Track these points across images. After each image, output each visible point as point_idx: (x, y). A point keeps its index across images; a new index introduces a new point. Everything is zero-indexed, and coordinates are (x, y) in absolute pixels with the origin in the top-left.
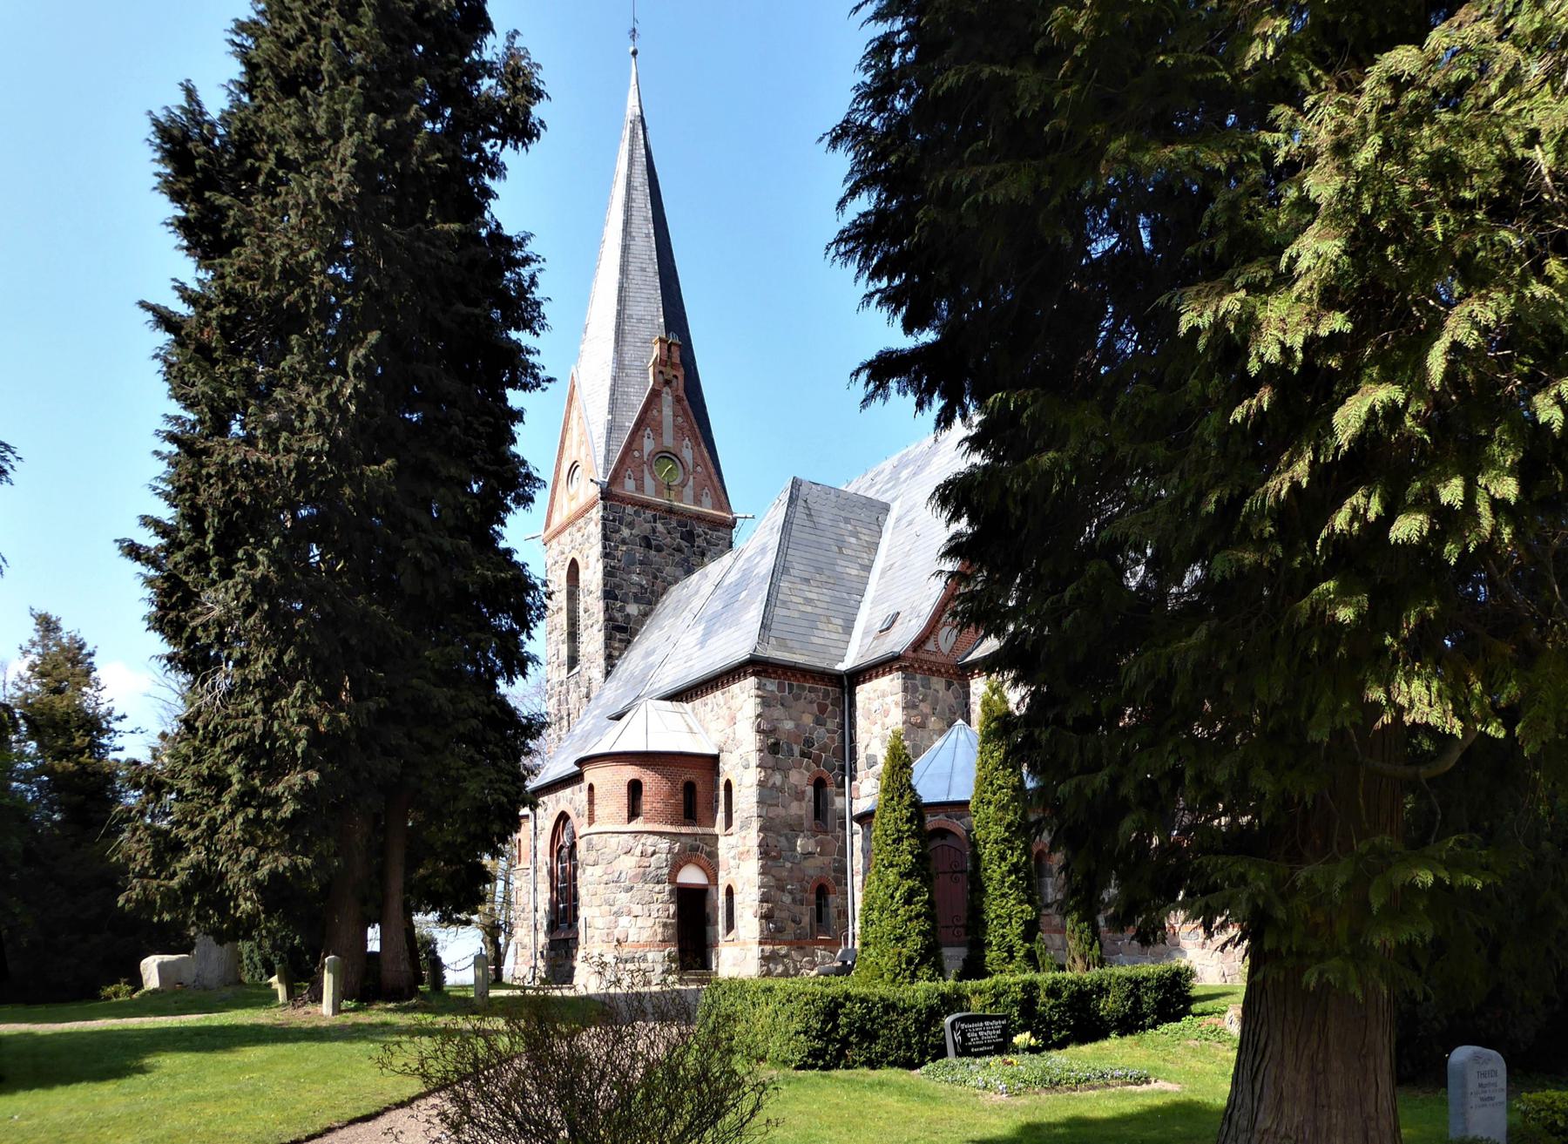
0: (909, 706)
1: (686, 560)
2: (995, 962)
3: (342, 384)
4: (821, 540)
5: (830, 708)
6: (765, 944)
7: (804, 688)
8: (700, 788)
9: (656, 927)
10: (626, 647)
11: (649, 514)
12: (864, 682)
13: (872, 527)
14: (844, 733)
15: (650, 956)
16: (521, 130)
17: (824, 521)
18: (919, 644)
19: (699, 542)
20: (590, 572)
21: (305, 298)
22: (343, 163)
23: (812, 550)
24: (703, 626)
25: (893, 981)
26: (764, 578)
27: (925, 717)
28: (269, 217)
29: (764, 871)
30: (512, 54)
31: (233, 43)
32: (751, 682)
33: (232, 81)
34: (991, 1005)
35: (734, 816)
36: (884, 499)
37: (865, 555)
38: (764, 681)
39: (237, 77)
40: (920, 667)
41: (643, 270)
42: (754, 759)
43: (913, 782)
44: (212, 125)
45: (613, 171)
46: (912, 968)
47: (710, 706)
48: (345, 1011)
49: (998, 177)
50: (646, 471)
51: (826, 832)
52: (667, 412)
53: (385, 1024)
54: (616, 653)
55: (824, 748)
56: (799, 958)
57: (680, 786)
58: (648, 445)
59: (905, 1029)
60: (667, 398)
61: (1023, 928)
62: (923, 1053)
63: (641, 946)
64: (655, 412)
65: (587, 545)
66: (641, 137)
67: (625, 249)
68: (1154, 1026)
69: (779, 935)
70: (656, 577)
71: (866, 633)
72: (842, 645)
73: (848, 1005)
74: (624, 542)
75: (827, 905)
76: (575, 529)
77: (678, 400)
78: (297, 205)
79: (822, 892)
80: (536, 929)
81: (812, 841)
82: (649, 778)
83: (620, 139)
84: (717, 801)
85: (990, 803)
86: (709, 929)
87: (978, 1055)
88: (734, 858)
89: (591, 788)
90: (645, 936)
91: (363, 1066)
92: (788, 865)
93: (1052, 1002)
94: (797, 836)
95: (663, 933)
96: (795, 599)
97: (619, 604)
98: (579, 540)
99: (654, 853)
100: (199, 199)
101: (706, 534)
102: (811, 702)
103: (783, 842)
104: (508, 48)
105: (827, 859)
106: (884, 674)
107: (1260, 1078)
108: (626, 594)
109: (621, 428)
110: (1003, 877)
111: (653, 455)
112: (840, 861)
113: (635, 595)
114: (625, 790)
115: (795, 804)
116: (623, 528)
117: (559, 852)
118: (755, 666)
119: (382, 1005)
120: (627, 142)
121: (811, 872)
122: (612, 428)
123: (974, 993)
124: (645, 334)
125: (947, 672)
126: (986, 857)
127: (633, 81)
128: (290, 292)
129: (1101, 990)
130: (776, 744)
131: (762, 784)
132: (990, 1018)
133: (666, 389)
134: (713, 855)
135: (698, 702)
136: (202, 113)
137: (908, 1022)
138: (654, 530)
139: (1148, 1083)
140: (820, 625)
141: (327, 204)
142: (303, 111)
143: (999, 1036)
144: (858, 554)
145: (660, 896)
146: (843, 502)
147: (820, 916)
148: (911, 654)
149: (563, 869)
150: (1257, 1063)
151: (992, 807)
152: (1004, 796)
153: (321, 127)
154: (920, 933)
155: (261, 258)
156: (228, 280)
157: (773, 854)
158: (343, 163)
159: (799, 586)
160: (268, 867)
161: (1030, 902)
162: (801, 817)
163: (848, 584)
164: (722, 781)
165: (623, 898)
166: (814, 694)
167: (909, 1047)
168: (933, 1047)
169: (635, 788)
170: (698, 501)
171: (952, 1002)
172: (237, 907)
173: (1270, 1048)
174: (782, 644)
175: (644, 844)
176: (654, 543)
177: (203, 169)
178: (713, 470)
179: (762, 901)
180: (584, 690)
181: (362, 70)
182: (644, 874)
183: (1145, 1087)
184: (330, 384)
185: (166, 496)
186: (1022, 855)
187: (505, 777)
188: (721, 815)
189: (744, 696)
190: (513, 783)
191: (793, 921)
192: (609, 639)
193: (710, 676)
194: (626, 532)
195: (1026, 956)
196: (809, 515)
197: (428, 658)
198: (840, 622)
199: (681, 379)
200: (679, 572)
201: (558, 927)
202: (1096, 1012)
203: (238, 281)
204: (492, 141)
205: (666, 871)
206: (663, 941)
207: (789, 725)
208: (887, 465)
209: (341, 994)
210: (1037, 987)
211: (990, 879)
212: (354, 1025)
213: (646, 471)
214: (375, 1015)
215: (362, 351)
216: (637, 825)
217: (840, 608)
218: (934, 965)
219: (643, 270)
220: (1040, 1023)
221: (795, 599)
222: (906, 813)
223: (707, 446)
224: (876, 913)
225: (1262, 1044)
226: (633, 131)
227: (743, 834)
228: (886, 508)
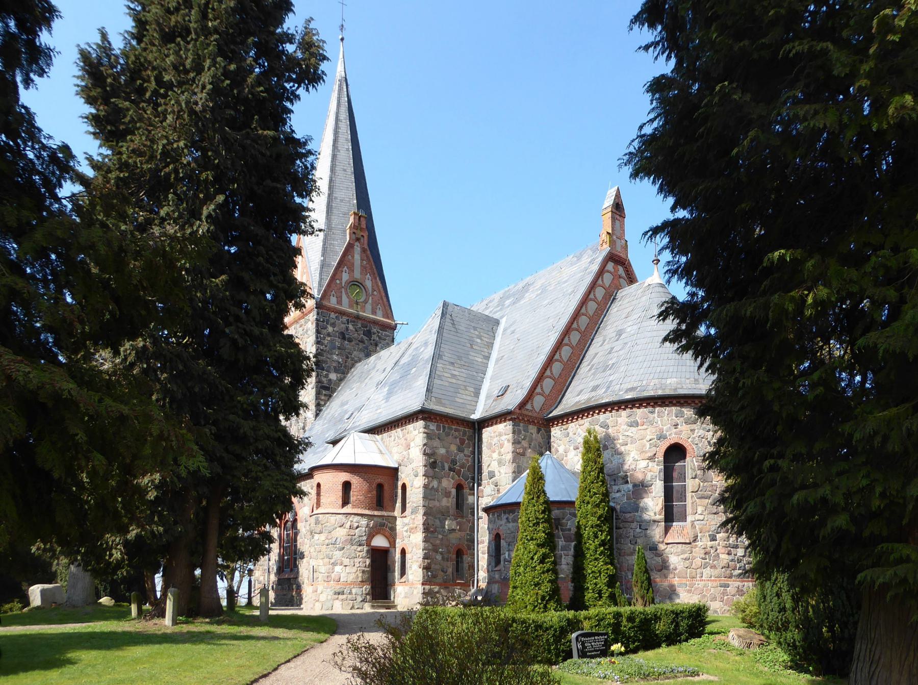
0: (516, 442)
1: (366, 348)
2: (591, 600)
3: (199, 226)
4: (460, 339)
5: (467, 442)
6: (426, 584)
7: (452, 429)
8: (386, 487)
9: (358, 573)
10: (328, 400)
11: (345, 319)
12: (487, 427)
13: (489, 333)
14: (474, 457)
15: (354, 591)
16: (312, 77)
17: (462, 328)
18: (522, 405)
19: (374, 337)
21: (176, 171)
22: (204, 87)
23: (454, 345)
24: (387, 389)
25: (533, 610)
26: (427, 361)
27: (525, 449)
28: (153, 118)
29: (426, 540)
30: (308, 32)
31: (129, 7)
32: (420, 424)
33: (126, 32)
34: (596, 626)
35: (407, 505)
36: (496, 316)
37: (486, 350)
38: (429, 423)
39: (130, 29)
40: (523, 419)
41: (345, 170)
42: (421, 471)
43: (545, 489)
44: (117, 57)
45: (327, 109)
46: (545, 602)
47: (393, 438)
48: (180, 623)
49: (816, 113)
50: (343, 292)
51: (462, 517)
52: (357, 257)
53: (208, 632)
54: (322, 403)
55: (462, 466)
56: (445, 594)
57: (374, 486)
58: (345, 277)
59: (548, 640)
60: (357, 249)
61: (607, 579)
62: (557, 656)
63: (348, 584)
64: (350, 257)
65: (306, 335)
66: (345, 90)
67: (334, 157)
68: (686, 640)
69: (434, 580)
70: (347, 358)
71: (488, 397)
72: (473, 403)
73: (515, 625)
74: (329, 335)
75: (462, 562)
76: (298, 325)
77: (364, 251)
78: (173, 112)
79: (459, 553)
80: (269, 572)
81: (454, 522)
82: (355, 481)
83: (332, 90)
84: (396, 496)
85: (588, 503)
86: (389, 574)
87: (593, 657)
88: (406, 531)
89: (319, 485)
90: (351, 578)
91: (210, 660)
92: (440, 536)
93: (630, 625)
94: (446, 519)
95: (362, 577)
96: (446, 375)
97: (325, 373)
98: (301, 332)
99: (357, 527)
100: (106, 102)
101: (378, 332)
102: (456, 438)
103: (438, 523)
104: (306, 28)
105: (463, 534)
106: (500, 423)
107: (875, 678)
108: (329, 367)
109: (329, 265)
110: (596, 548)
111: (348, 283)
112: (470, 535)
113: (335, 368)
114: (340, 487)
115: (445, 500)
116: (329, 326)
117: (285, 524)
118: (424, 414)
119: (201, 620)
120: (336, 92)
121: (454, 541)
122: (323, 265)
123: (585, 618)
124: (345, 209)
125: (538, 422)
126: (585, 536)
127: (341, 56)
128: (167, 165)
129: (656, 618)
130: (435, 462)
131: (426, 487)
132: (598, 635)
133: (357, 244)
134: (393, 529)
135: (385, 435)
136: (111, 49)
137: (549, 636)
138: (347, 329)
139: (698, 675)
140: (461, 391)
141: (192, 112)
142: (177, 53)
143: (603, 645)
144: (482, 349)
145: (361, 553)
146: (473, 317)
147: (458, 568)
148: (518, 411)
149: (288, 535)
150: (873, 669)
151: (590, 506)
152: (597, 499)
153: (188, 63)
154: (550, 581)
155: (149, 143)
156: (125, 156)
157: (432, 529)
158: (204, 87)
159: (448, 367)
160: (135, 532)
161: (612, 564)
162: (448, 507)
163: (477, 367)
164: (400, 484)
165: (338, 554)
166: (459, 431)
167: (549, 651)
168: (563, 651)
169: (347, 486)
170: (374, 313)
171: (573, 625)
172: (111, 555)
173: (882, 660)
174: (439, 401)
175: (351, 521)
176: (347, 336)
177: (111, 85)
178: (383, 294)
179: (424, 558)
180: (301, 425)
181: (216, 31)
182: (351, 540)
183: (696, 679)
184: (192, 226)
186: (607, 535)
187: (285, 477)
188: (399, 505)
189: (416, 432)
190: (291, 481)
191: (443, 571)
192: (318, 394)
193: (395, 419)
194: (330, 329)
195: (609, 596)
196: (453, 324)
197: (239, 402)
198: (472, 389)
199: (366, 237)
200: (362, 355)
201: (283, 571)
202: (654, 632)
203: (131, 157)
204: (291, 84)
205: (365, 538)
206: (362, 582)
207: (442, 451)
208: (497, 297)
209: (178, 612)
210: (622, 616)
211: (588, 549)
212: (188, 632)
213: (343, 292)
214: (200, 626)
215: (212, 207)
216: (348, 509)
217: (472, 381)
218: (557, 601)
219: (345, 170)
220: (623, 638)
221: (446, 375)
222: (542, 508)
223: (380, 279)
224: (522, 569)
225: (877, 657)
226: (340, 86)
227: (413, 517)
228: (497, 322)
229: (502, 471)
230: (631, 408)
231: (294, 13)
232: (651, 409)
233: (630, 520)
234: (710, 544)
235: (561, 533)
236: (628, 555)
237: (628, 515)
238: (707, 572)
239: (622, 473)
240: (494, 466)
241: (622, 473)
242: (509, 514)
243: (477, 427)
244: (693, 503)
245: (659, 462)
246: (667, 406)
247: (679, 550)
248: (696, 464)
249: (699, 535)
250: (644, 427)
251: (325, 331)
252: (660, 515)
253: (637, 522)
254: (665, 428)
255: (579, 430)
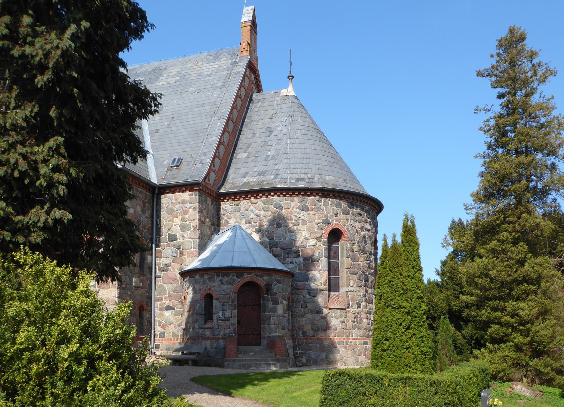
51: (144, 275)
94: (133, 276)
106: (184, 191)
229: (186, 235)
230: (303, 195)
232: (318, 198)
233: (301, 287)
234: (357, 310)
235: (270, 297)
236: (299, 317)
237: (299, 284)
238: (356, 332)
239: (294, 248)
240: (176, 230)
241: (294, 248)
242: (223, 277)
243: (156, 192)
244: (347, 277)
245: (324, 242)
246: (331, 197)
247: (338, 314)
248: (349, 246)
249: (351, 303)
250: (313, 212)
252: (325, 285)
253: (307, 289)
254: (328, 215)
255: (252, 207)
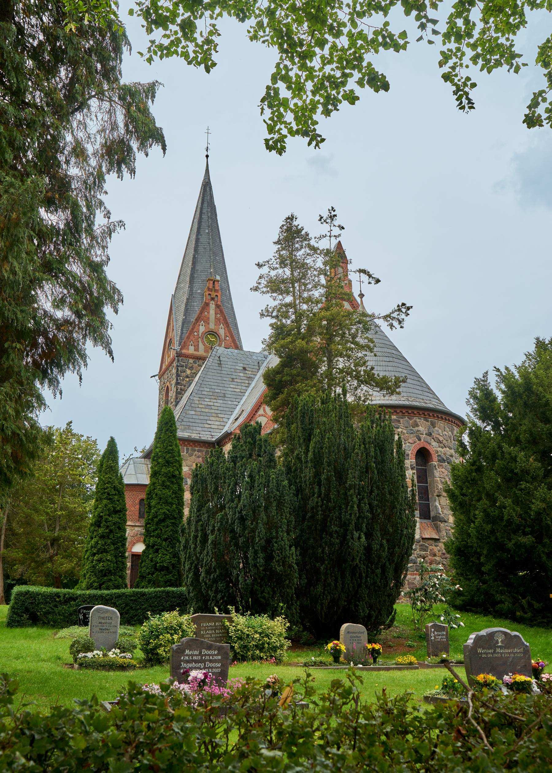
20: (172, 392)
57: (137, 501)
58: (202, 329)
64: (206, 313)
102: (198, 457)
109: (189, 322)
133: (212, 302)
144: (243, 381)
185: (83, 356)
231: (164, 148)
251: (183, 374)
